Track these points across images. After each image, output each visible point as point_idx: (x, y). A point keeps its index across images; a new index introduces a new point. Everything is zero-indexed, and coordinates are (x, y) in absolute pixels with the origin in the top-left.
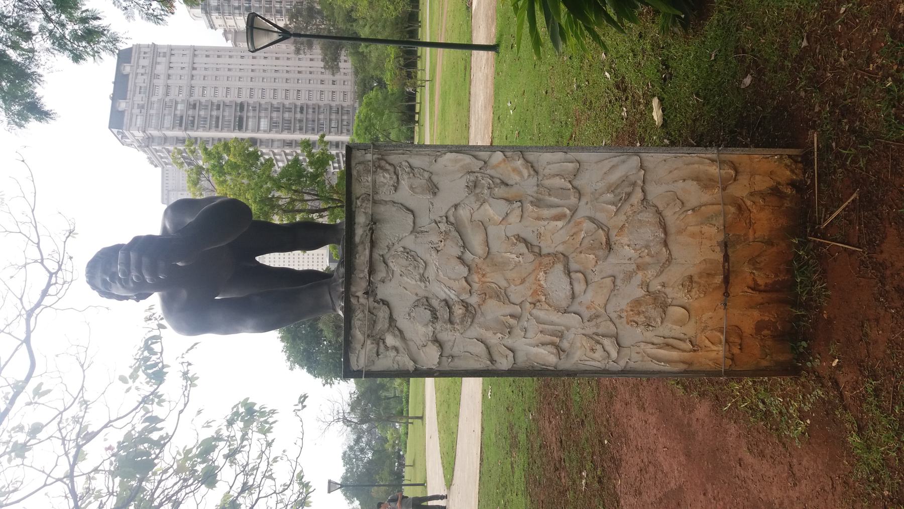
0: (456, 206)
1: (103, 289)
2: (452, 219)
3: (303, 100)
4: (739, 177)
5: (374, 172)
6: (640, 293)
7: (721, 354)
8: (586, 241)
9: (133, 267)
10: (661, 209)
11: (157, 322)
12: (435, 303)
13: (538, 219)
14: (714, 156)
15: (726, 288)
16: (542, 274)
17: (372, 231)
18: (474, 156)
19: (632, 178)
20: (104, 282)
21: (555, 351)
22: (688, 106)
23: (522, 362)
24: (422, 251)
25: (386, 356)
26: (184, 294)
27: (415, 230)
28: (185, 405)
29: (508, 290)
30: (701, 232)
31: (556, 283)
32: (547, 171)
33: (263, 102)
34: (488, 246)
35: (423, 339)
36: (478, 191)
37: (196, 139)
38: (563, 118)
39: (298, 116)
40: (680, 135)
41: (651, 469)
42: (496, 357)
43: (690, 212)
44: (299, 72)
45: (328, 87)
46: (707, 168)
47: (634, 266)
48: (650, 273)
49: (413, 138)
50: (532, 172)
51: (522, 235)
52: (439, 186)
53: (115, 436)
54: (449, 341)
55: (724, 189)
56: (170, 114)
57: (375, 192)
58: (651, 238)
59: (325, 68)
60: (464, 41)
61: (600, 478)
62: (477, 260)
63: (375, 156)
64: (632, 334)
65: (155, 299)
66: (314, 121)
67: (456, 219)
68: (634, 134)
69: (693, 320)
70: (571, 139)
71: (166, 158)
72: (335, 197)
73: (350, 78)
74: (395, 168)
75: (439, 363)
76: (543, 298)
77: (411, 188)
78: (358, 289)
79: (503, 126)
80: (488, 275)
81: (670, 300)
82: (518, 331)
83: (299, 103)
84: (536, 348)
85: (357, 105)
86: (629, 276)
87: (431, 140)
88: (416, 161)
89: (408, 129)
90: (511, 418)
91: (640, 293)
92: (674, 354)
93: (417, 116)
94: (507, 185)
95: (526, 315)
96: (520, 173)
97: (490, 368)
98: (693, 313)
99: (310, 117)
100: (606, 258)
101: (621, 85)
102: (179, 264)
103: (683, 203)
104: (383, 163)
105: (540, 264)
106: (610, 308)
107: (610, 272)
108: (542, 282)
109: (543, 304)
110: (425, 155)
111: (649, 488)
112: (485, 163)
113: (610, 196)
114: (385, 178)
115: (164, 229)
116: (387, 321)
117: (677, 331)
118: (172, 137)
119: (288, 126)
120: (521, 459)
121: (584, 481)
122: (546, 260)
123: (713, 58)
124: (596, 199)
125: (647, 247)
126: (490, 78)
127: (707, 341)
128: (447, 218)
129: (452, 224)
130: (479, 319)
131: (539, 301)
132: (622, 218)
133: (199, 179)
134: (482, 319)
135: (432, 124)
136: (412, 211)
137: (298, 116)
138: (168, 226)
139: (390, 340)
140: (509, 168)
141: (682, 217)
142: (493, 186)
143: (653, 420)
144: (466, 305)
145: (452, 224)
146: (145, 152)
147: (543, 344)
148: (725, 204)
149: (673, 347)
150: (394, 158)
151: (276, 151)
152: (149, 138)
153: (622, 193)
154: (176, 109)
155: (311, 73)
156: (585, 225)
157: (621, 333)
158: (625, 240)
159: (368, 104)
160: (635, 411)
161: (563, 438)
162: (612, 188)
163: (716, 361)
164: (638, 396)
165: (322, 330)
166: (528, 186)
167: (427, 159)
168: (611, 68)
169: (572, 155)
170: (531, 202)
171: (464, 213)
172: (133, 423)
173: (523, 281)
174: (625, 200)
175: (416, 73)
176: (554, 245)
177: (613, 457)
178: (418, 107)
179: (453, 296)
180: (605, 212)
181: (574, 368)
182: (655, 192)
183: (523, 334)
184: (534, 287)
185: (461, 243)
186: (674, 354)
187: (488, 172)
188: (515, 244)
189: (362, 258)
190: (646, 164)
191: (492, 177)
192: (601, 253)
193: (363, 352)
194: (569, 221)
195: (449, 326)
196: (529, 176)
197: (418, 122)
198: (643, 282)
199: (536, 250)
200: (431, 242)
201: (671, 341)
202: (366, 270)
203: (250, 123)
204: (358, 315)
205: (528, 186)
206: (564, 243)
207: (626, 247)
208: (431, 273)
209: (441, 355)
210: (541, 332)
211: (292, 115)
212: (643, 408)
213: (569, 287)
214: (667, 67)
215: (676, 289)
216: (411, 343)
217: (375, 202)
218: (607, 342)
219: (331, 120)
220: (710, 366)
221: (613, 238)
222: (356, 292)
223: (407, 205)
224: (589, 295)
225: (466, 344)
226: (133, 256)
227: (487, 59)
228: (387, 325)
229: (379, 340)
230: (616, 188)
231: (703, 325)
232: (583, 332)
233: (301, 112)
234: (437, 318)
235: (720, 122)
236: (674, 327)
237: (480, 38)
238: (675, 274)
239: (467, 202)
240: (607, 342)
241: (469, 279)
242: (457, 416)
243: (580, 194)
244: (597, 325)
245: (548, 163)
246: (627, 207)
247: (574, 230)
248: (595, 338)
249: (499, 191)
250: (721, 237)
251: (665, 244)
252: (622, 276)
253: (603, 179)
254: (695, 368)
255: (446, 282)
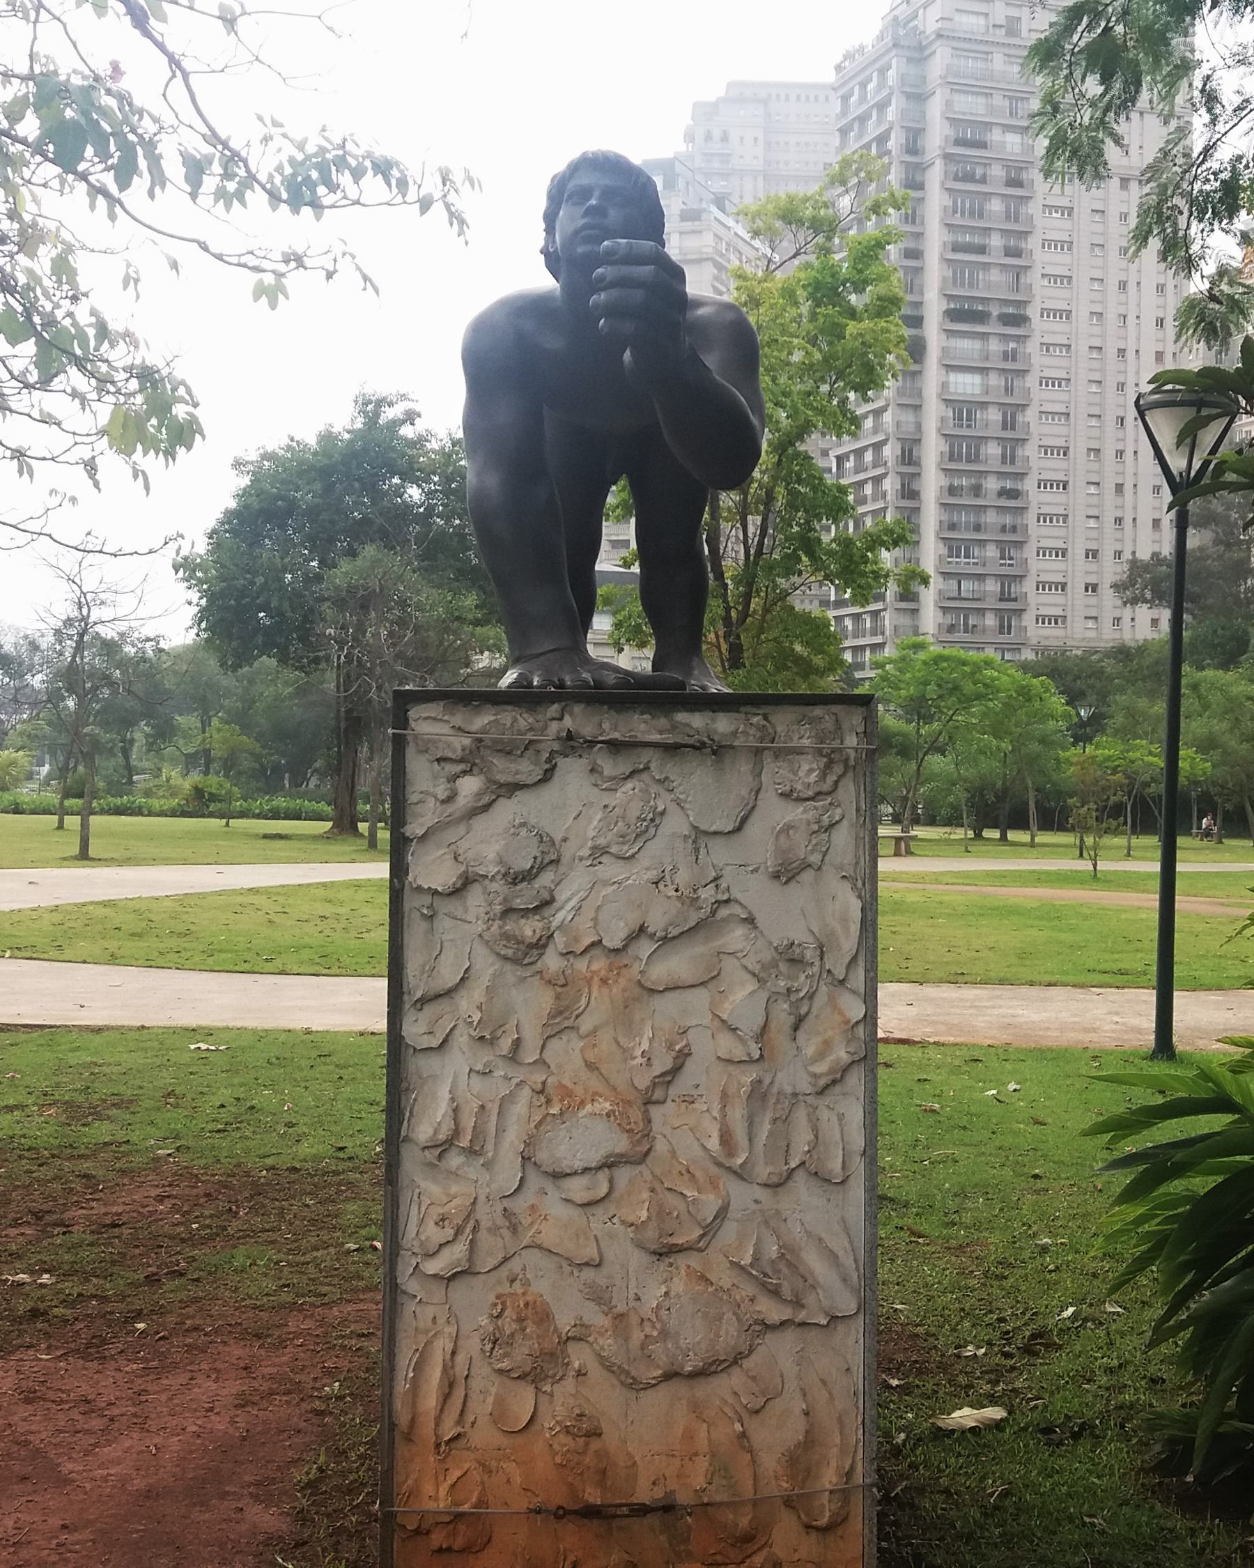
0: (750, 921)
1: (571, 186)
2: (723, 912)
3: (1038, 499)
4: (814, 1534)
5: (820, 752)
6: (564, 1322)
7: (431, 1506)
8: (672, 1200)
9: (625, 270)
10: (746, 1363)
11: (437, 195)
12: (546, 879)
13: (725, 1097)
14: (859, 1479)
15: (575, 1512)
16: (607, 1106)
17: (699, 747)
18: (854, 959)
19: (810, 1300)
20: (585, 193)
21: (442, 1137)
22: (983, 1478)
23: (419, 1066)
24: (656, 850)
25: (435, 777)
26: (553, 342)
27: (699, 836)
28: (219, 257)
29: (573, 1035)
30: (696, 1454)
31: (586, 1139)
32: (824, 1114)
33: (1031, 381)
34: (667, 989)
35: (470, 855)
36: (783, 967)
37: (921, 187)
38: (967, 1218)
39: (992, 484)
40: (913, 1466)
41: (96, 1423)
42: (430, 1011)
43: (738, 1427)
44: (1119, 488)
45: (1078, 571)
46: (833, 1464)
47: (621, 1308)
48: (608, 1344)
49: (932, 821)
50: (822, 1082)
51: (690, 1065)
52: (793, 884)
53: (144, 80)
54: (466, 910)
55: (789, 1503)
56: (991, 110)
57: (778, 754)
58: (682, 1343)
59: (1134, 563)
60: (1178, 971)
61: (45, 1313)
62: (637, 967)
63: (852, 754)
64: (474, 1306)
65: (543, 281)
66: (977, 528)
67: (723, 920)
68: (920, 1372)
69: (505, 1441)
70: (913, 1233)
71: (863, 98)
72: (755, 603)
73: (1107, 637)
74: (829, 793)
75: (419, 889)
76: (555, 1110)
77: (788, 828)
78: (578, 720)
79: (955, 1070)
80: (605, 991)
81: (547, 1388)
82: (484, 1057)
83: (1029, 485)
84: (448, 1096)
85: (1028, 655)
86: (599, 1297)
87: (895, 877)
88: (843, 838)
89: (956, 808)
90: (148, 1103)
91: (564, 1322)
92: (430, 1401)
93: (996, 834)
94: (796, 1028)
95: (519, 1074)
96: (821, 1055)
97: (406, 997)
98: (519, 1440)
99: (991, 518)
100: (640, 1245)
101: (1039, 1343)
102: (627, 356)
103: (757, 1412)
104: (838, 769)
105: (629, 1103)
106: (532, 1257)
107: (609, 1256)
108: (589, 1107)
109: (543, 1110)
110: (857, 857)
111: (47, 1418)
112: (842, 982)
113: (772, 1250)
114: (807, 772)
115: (698, 304)
116: (510, 779)
117: (481, 1408)
118: (923, 114)
119: (962, 450)
120: (42, 1128)
121: (23, 1277)
122: (636, 1114)
123: (1087, 1520)
124: (766, 1223)
125: (664, 1334)
126: (1087, 1037)
127: (458, 1473)
128: (727, 901)
129: (713, 913)
130: (511, 973)
131: (549, 1101)
132: (724, 1277)
133: (800, 222)
134: (511, 978)
135: (968, 878)
136: (739, 829)
137: (992, 484)
138: (701, 311)
139: (469, 786)
140: (830, 1033)
141: (727, 1410)
142: (793, 998)
143: (219, 1424)
144: (541, 945)
145: (713, 913)
146: (881, 37)
147: (456, 1110)
148: (755, 1503)
149: (446, 1398)
150: (848, 792)
151: (887, 417)
152: (921, 48)
153: (778, 1276)
154: (1007, 128)
155: (1119, 521)
156: (712, 1197)
157: (478, 1282)
158: (678, 1286)
159: (1025, 693)
160: (233, 1386)
161: (126, 1231)
162: (789, 1257)
163: (413, 1493)
164: (272, 1393)
165: (352, 553)
166: (793, 1076)
167: (849, 859)
168: (1085, 1320)
169: (858, 1166)
170: (760, 1082)
171: (736, 937)
172: (182, 129)
173: (591, 1066)
174: (763, 1285)
175: (1116, 832)
176: (668, 1131)
177: (104, 1342)
178: (1023, 837)
179: (560, 916)
180: (739, 1242)
181: (404, 1180)
182: (781, 1351)
183: (479, 1067)
184: (579, 1091)
185: (674, 932)
186: (430, 1401)
187: (823, 989)
188: (670, 1047)
189: (643, 726)
190: (841, 1328)
191: (811, 996)
192: (651, 1234)
193: (446, 729)
194: (719, 1164)
195: (498, 909)
196: (815, 1076)
197: (978, 836)
198: (588, 1327)
199: (658, 1094)
200: (675, 869)
201: (459, 1393)
202: (616, 735)
203: (966, 344)
204: (524, 720)
205: (793, 1076)
206: (673, 1153)
207: (664, 1289)
208: (610, 869)
209: (435, 893)
210: (482, 1107)
211: (995, 465)
212: (243, 1402)
213: (578, 1165)
214: (1076, 1436)
215: (571, 1401)
216: (462, 829)
217: (758, 752)
218: (458, 1251)
219: (981, 577)
220: (405, 1480)
221: (681, 1261)
222: (571, 715)
223: (754, 818)
224: (555, 1209)
225: (458, 946)
226: (646, 271)
227: (1140, 1031)
228: (502, 778)
229: (470, 762)
230: (790, 1264)
231: (494, 1463)
232: (482, 1198)
233: (1003, 493)
234: (514, 883)
235: (942, 1539)
236: (490, 1400)
237: (1190, 1011)
238: (604, 1399)
239: (759, 944)
240: (458, 1251)
241: (596, 952)
242: (113, 959)
243: (777, 1185)
244: (494, 1230)
245: (841, 1117)
246: (749, 1289)
247: (698, 1174)
248: (466, 1225)
249: (782, 1014)
250: (684, 1498)
251: (671, 1375)
252: (602, 1282)
253: (809, 1234)
254: (401, 1450)
255: (591, 900)
